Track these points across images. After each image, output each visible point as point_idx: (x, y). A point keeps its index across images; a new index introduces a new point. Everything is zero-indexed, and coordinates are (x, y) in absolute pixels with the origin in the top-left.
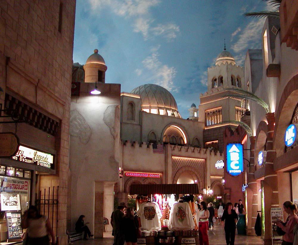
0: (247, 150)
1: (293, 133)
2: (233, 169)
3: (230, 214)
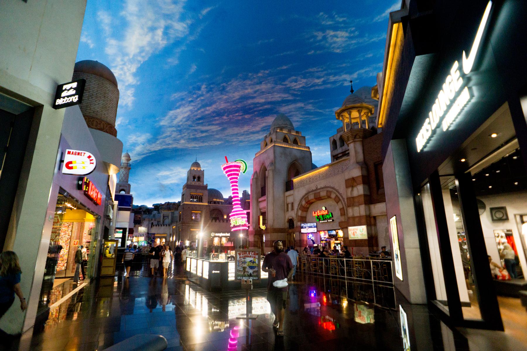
2: (259, 191)
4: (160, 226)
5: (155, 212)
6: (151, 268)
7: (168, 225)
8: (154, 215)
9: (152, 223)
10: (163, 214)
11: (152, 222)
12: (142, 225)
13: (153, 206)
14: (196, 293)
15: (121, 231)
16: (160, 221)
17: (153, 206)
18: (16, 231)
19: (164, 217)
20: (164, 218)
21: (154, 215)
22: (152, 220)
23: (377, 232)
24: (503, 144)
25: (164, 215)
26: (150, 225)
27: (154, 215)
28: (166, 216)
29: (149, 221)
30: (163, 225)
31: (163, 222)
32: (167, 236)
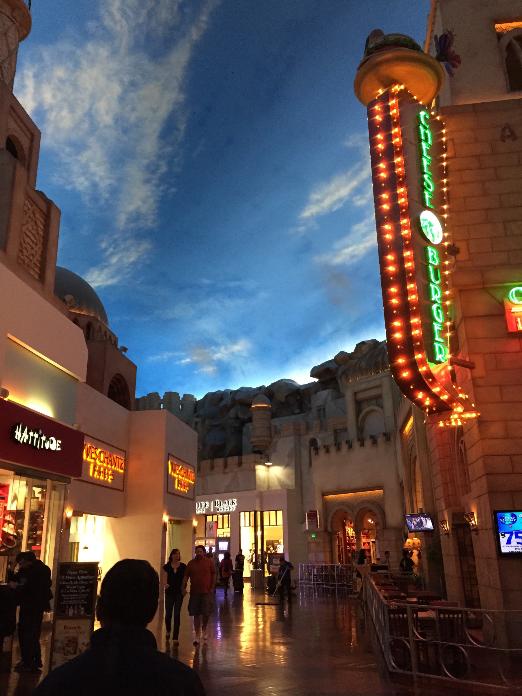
0: (411, 454)
1: (190, 614)
3: (254, 470)
4: (344, 447)
5: (324, 394)
6: (398, 606)
7: (381, 440)
8: (321, 410)
9: (313, 443)
10: (355, 394)
11: (311, 436)
12: (272, 457)
13: (313, 375)
14: (487, 493)
15: (32, 500)
16: (345, 430)
17: (314, 374)
18: (416, 496)
19: (359, 404)
20: (358, 412)
21: (319, 410)
22: (308, 428)
23: (193, 536)
24: (167, 635)
25: (360, 396)
26: (305, 453)
27: (321, 410)
28: (369, 400)
29: (298, 434)
30: (356, 444)
31: (360, 430)
32: (383, 498)
